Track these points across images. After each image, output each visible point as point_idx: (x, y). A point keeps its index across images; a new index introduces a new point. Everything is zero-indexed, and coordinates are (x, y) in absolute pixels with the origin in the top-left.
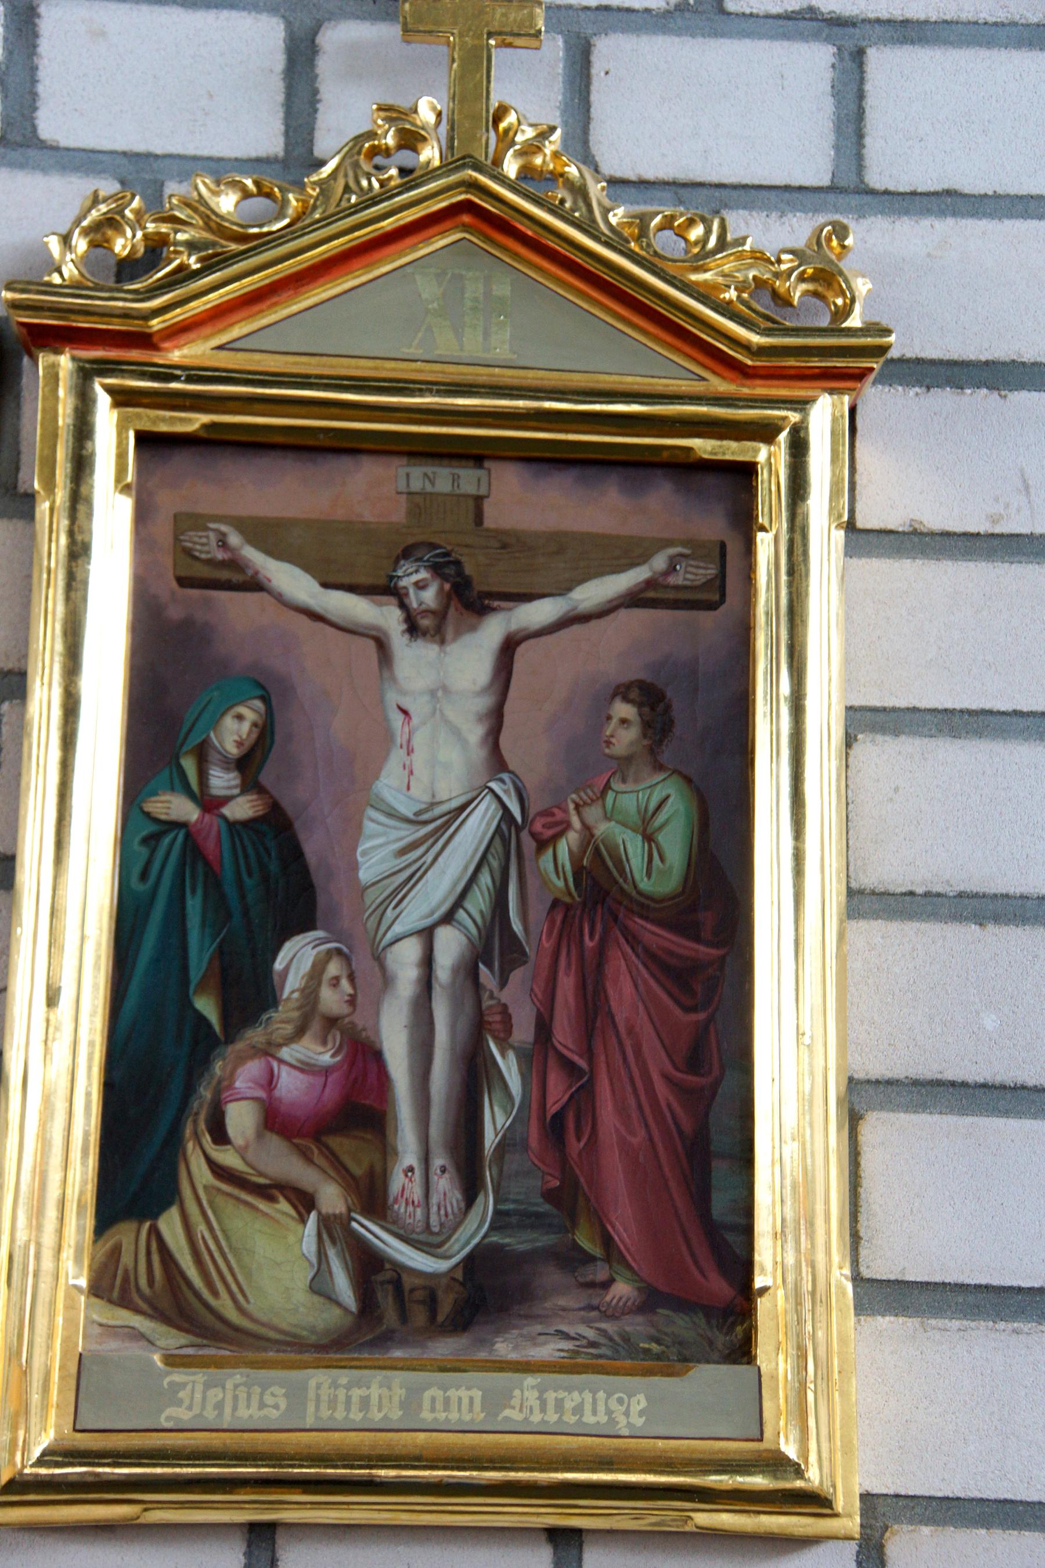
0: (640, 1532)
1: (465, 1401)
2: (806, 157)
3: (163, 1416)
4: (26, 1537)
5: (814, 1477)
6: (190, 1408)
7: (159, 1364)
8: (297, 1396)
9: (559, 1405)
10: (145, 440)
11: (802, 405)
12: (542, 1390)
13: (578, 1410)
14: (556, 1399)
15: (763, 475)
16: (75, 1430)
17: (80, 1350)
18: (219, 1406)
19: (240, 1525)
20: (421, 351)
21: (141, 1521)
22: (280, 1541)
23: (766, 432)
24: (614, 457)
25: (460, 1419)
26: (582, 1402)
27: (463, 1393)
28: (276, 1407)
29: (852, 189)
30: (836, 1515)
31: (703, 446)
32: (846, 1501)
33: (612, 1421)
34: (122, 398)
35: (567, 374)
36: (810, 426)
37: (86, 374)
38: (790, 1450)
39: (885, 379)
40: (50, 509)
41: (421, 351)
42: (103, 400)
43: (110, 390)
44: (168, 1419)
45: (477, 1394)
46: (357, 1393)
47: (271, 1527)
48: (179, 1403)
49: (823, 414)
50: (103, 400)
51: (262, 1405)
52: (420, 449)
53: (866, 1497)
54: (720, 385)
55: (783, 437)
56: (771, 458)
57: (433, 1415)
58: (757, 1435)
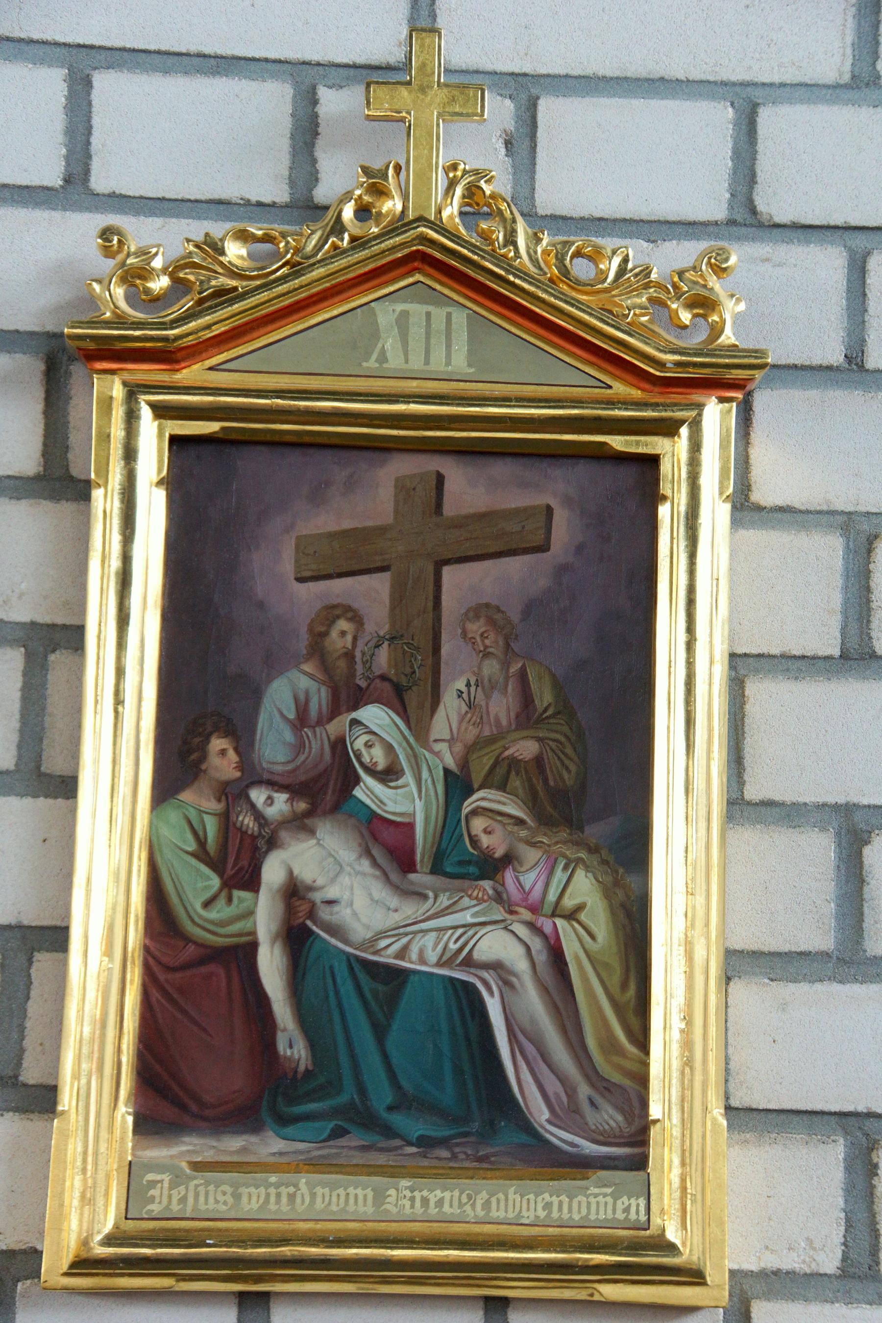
0: (351, 1294)
1: (361, 1198)
2: (705, 196)
3: (144, 1211)
4: (96, 1301)
5: (688, 1256)
6: (160, 1203)
7: (188, 1171)
8: (380, 1197)
9: (425, 1201)
10: (175, 440)
11: (700, 406)
12: (311, 1186)
13: (440, 1203)
14: (422, 1196)
15: (665, 467)
16: (126, 1218)
17: (130, 1158)
18: (183, 1200)
19: (233, 1293)
20: (472, 370)
21: (177, 1289)
22: (272, 1300)
23: (669, 429)
24: (376, 444)
25: (355, 1210)
26: (630, 1204)
27: (359, 1191)
28: (225, 1203)
29: (747, 219)
30: (704, 1284)
31: (618, 442)
32: (717, 1276)
33: (519, 1215)
34: (161, 412)
35: (474, 384)
36: (704, 423)
37: (132, 391)
38: (673, 1235)
39: (768, 383)
40: (105, 501)
41: (472, 370)
42: (146, 413)
43: (153, 406)
44: (146, 1213)
45: (370, 1193)
46: (284, 1191)
47: (505, 1302)
48: (152, 1200)
49: (715, 415)
50: (146, 413)
51: (217, 1202)
52: (415, 447)
53: (732, 1273)
54: (620, 389)
55: (684, 431)
56: (673, 452)
57: (277, 1207)
58: (129, 1216)
